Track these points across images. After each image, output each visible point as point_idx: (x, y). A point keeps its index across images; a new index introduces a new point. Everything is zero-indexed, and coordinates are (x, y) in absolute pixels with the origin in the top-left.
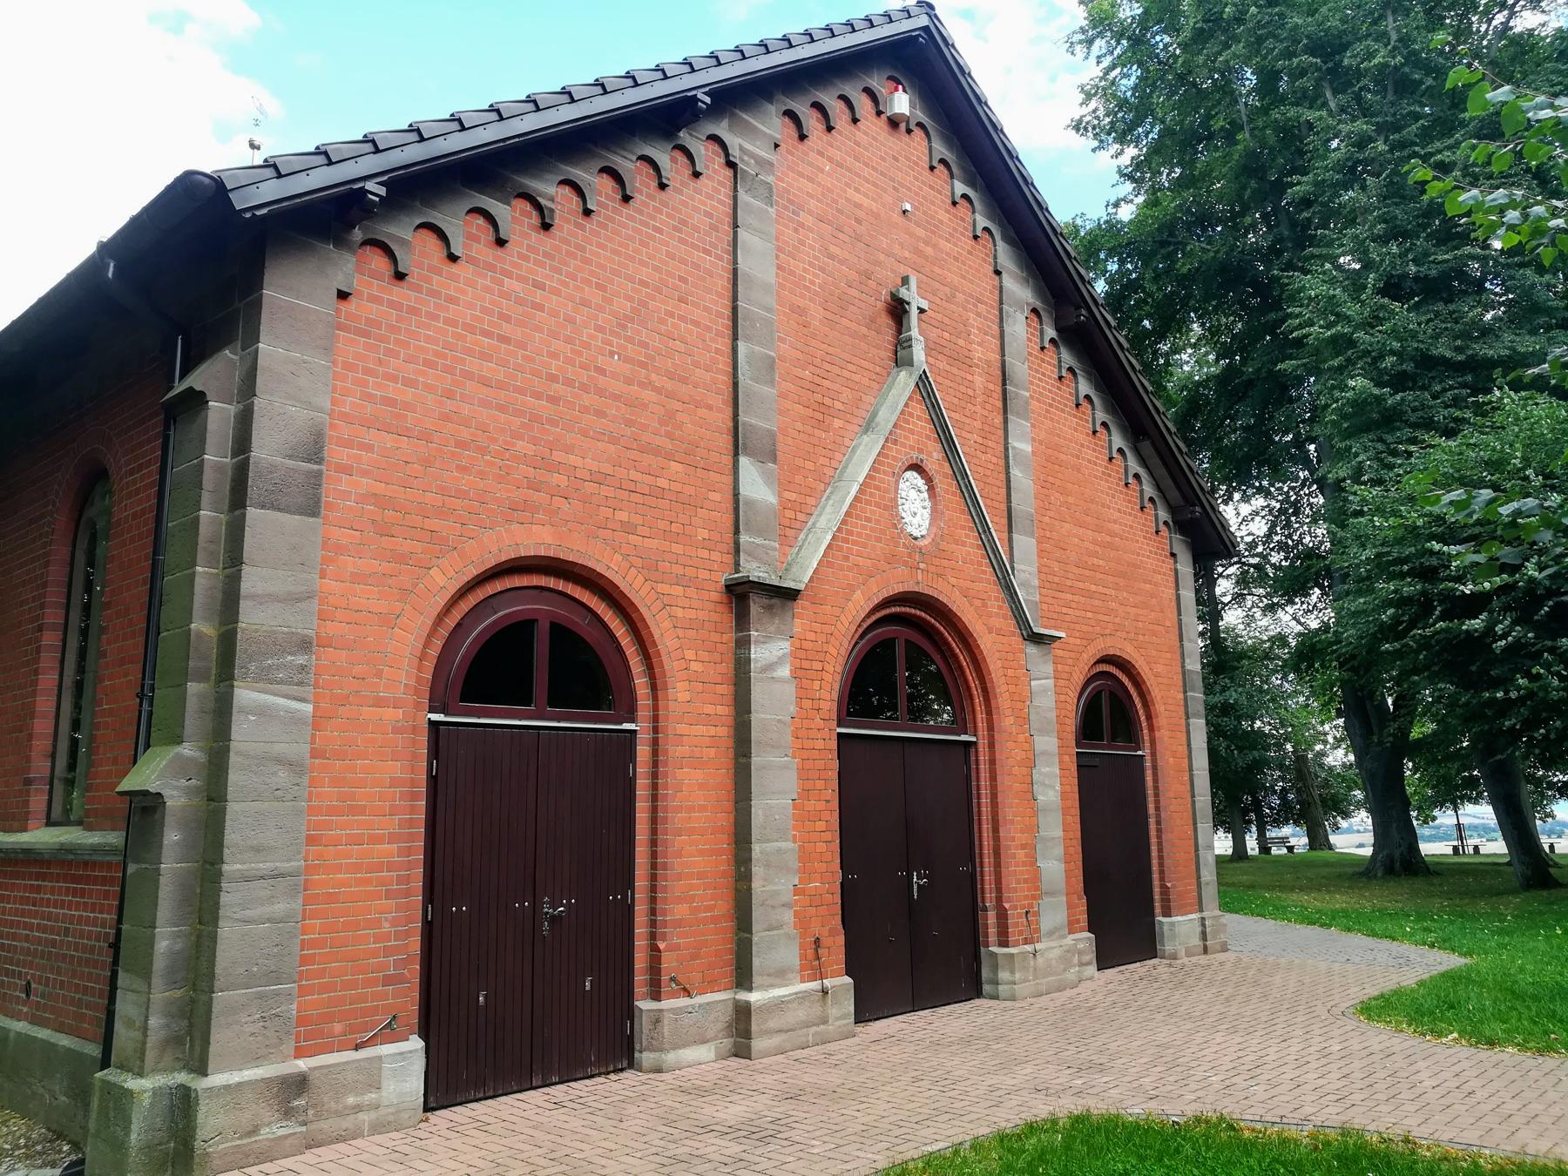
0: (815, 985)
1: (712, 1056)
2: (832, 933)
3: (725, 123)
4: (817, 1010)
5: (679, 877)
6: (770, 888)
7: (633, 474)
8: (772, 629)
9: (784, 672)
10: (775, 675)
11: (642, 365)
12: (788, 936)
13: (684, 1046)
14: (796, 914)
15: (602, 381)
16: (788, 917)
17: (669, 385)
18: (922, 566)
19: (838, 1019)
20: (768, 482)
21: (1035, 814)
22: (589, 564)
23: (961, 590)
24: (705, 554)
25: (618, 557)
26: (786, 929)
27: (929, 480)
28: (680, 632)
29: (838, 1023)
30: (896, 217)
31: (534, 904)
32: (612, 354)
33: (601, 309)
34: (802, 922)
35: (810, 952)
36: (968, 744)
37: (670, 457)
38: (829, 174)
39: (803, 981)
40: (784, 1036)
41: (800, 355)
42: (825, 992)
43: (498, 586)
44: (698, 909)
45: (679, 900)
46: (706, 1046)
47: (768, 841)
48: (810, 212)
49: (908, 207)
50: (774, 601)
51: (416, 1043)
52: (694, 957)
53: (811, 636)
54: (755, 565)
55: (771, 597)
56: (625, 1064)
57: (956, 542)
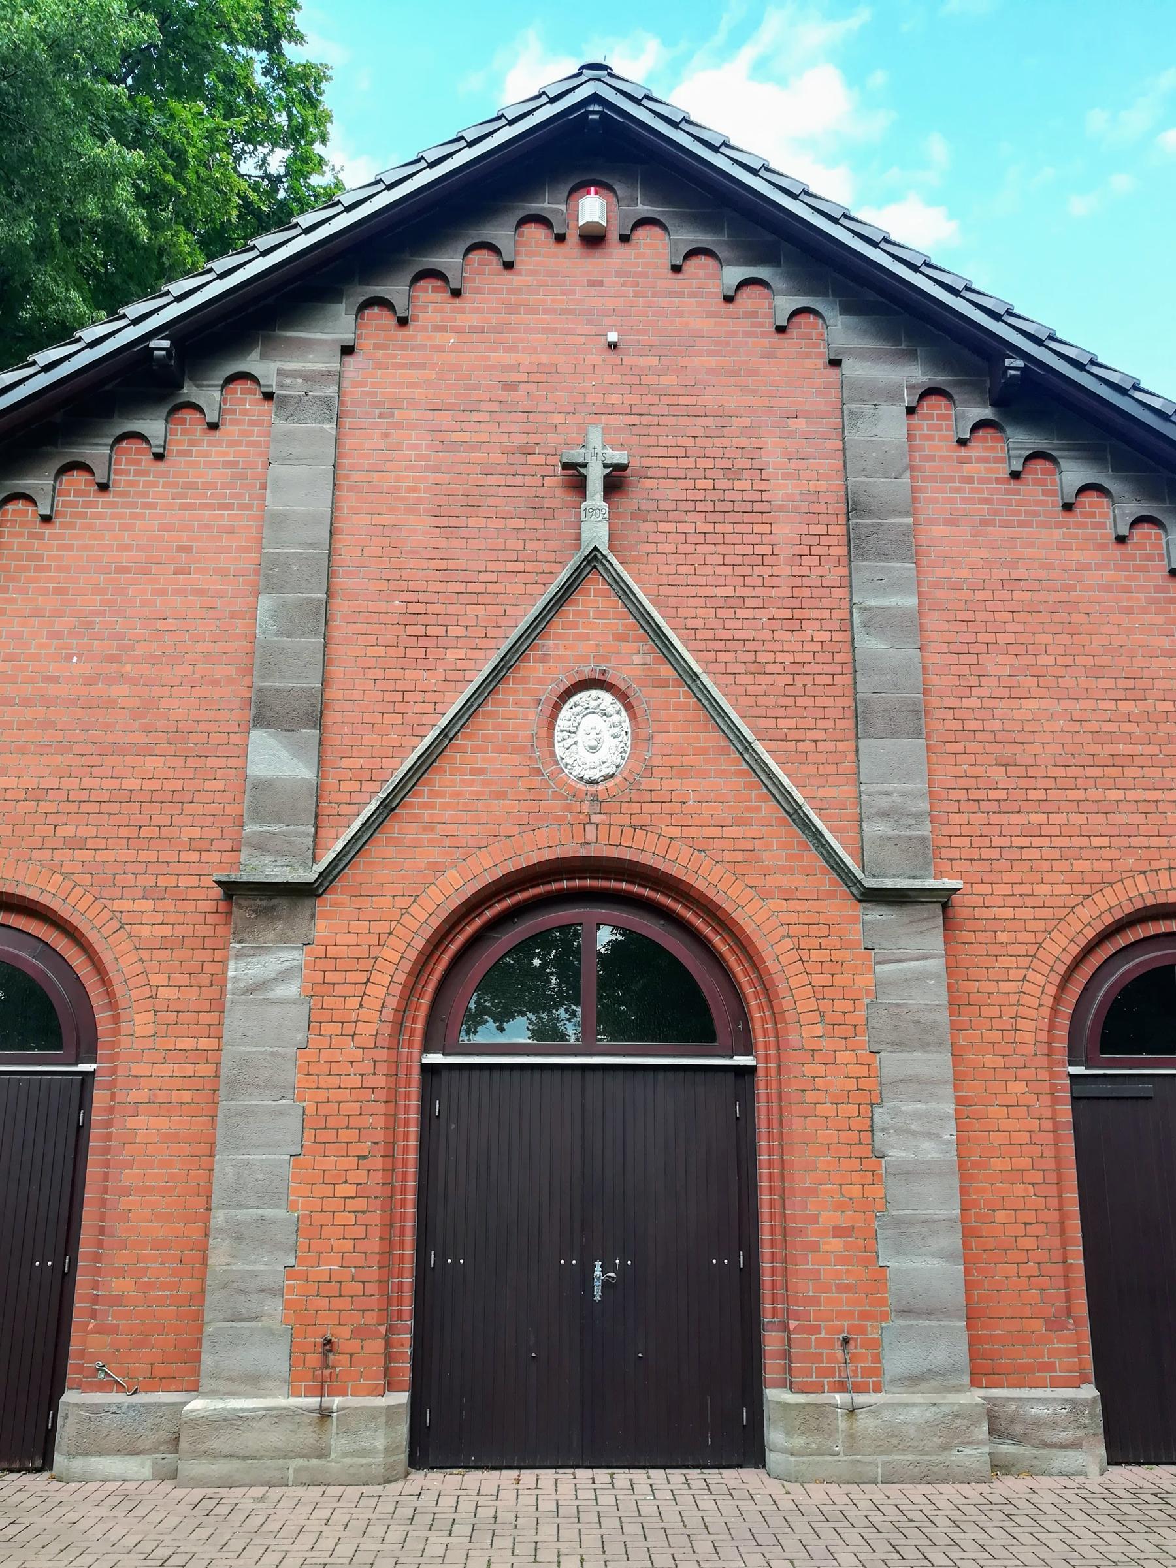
0: (313, 1402)
1: (147, 1472)
2: (359, 1334)
3: (255, 354)
4: (307, 1436)
5: (123, 1245)
6: (240, 1266)
7: (87, 782)
8: (271, 936)
9: (291, 989)
10: (271, 995)
11: (111, 659)
12: (270, 1332)
13: (100, 1453)
14: (288, 1304)
15: (51, 690)
16: (274, 1307)
17: (149, 671)
18: (595, 819)
19: (345, 1454)
20: (296, 755)
21: (877, 1179)
22: (17, 891)
23: (691, 842)
24: (194, 857)
25: (58, 878)
26: (265, 1322)
27: (622, 696)
28: (145, 955)
29: (348, 1460)
30: (598, 358)
31: (581, 1262)
32: (69, 658)
33: (59, 613)
34: (301, 1314)
35: (314, 1359)
36: (751, 1070)
37: (146, 751)
38: (454, 348)
39: (295, 1393)
40: (236, 1464)
41: (383, 585)
42: (324, 1414)
43: (1110, 948)
44: (150, 1285)
45: (120, 1273)
46: (139, 1458)
47: (240, 1206)
48: (413, 406)
49: (613, 337)
50: (275, 902)
51: (1089, 1392)
52: (139, 1344)
53: (343, 939)
54: (267, 859)
55: (271, 897)
56: (38, 1463)
57: (683, 774)
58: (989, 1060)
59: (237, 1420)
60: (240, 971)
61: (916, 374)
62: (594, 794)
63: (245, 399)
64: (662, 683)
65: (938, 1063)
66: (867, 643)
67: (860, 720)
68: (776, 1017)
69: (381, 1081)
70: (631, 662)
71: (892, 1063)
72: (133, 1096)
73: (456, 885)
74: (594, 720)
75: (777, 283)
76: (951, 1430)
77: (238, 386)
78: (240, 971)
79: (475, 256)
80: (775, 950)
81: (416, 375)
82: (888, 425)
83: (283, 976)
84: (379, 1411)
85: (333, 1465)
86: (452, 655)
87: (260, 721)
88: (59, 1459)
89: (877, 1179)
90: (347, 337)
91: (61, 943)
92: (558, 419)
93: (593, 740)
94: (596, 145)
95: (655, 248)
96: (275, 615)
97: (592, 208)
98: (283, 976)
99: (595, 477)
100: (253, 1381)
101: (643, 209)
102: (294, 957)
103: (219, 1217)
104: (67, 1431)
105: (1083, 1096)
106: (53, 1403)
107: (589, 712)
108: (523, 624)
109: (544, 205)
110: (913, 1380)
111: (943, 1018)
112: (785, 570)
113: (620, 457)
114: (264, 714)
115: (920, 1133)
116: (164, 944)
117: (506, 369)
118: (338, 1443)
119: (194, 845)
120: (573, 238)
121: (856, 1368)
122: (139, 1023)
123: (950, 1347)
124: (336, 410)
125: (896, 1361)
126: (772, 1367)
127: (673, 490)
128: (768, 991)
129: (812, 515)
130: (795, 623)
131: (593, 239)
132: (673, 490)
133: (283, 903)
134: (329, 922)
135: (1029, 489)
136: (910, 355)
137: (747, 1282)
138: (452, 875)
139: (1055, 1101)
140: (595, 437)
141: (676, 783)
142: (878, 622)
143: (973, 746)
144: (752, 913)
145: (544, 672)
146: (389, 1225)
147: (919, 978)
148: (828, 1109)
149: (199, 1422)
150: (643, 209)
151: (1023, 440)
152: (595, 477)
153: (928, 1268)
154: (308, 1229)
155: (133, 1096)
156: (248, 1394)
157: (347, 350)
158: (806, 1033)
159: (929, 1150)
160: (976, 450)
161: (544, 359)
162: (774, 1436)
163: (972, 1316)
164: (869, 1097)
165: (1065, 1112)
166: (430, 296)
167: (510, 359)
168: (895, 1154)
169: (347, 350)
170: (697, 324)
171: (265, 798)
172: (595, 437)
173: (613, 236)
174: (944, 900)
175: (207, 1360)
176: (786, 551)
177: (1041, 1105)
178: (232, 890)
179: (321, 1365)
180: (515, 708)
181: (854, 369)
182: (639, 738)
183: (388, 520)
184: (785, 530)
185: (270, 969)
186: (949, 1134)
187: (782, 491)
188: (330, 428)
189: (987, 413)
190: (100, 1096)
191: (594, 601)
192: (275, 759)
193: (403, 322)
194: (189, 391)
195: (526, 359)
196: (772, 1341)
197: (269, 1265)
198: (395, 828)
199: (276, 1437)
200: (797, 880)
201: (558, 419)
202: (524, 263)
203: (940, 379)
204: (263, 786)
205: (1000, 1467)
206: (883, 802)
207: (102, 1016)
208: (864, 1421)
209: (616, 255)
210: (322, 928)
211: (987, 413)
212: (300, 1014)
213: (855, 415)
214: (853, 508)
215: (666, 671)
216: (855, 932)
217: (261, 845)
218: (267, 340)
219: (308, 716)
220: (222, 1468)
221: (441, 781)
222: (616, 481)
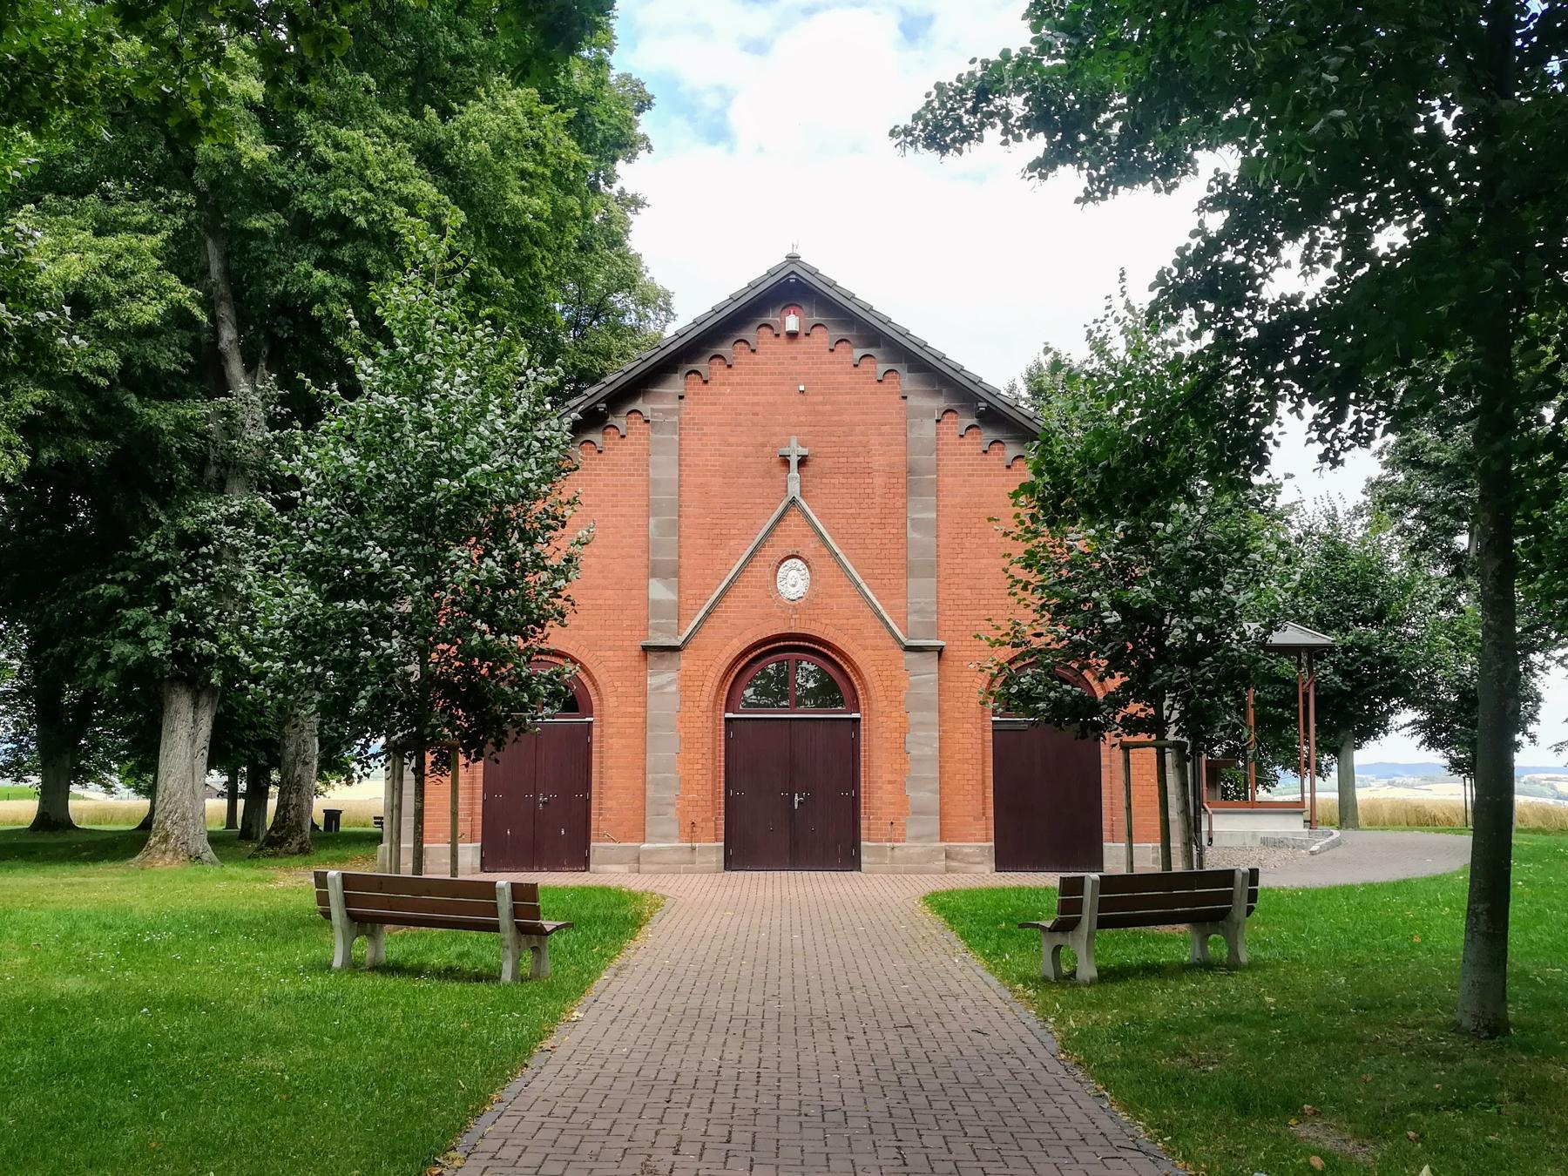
3: (640, 401)
4: (687, 857)
9: (673, 688)
16: (672, 811)
27: (806, 562)
35: (688, 829)
42: (693, 849)
57: (831, 596)
58: (957, 715)
59: (660, 851)
60: (652, 681)
61: (941, 403)
62: (794, 606)
63: (638, 422)
64: (822, 556)
65: (934, 716)
66: (913, 535)
67: (908, 570)
68: (869, 698)
69: (710, 724)
70: (810, 547)
71: (914, 717)
72: (611, 731)
73: (737, 645)
74: (793, 573)
75: (879, 357)
76: (931, 856)
77: (633, 415)
78: (652, 681)
79: (738, 345)
80: (868, 672)
81: (713, 409)
82: (928, 429)
83: (669, 683)
84: (713, 849)
85: (697, 866)
86: (732, 543)
87: (654, 575)
88: (592, 866)
89: (906, 762)
90: (681, 391)
91: (588, 684)
92: (777, 429)
93: (793, 581)
94: (792, 289)
95: (822, 338)
96: (657, 526)
97: (792, 323)
98: (669, 683)
99: (794, 461)
100: (665, 837)
101: (816, 319)
102: (673, 675)
103: (649, 777)
104: (595, 855)
105: (998, 730)
106: (587, 847)
107: (792, 569)
108: (765, 529)
109: (770, 318)
110: (918, 838)
111: (936, 698)
112: (878, 500)
113: (805, 452)
114: (654, 571)
115: (924, 743)
116: (619, 669)
117: (754, 404)
118: (698, 859)
119: (629, 628)
120: (783, 335)
121: (895, 831)
122: (611, 702)
123: (934, 825)
124: (680, 428)
125: (910, 832)
126: (1106, 835)
127: (829, 463)
128: (865, 688)
129: (891, 475)
130: (882, 526)
131: (793, 335)
132: (829, 463)
133: (668, 654)
134: (684, 661)
135: (992, 459)
136: (939, 393)
137: (856, 801)
138: (735, 641)
139: (984, 731)
140: (794, 441)
141: (829, 600)
142: (917, 524)
143: (957, 580)
144: (858, 656)
145: (773, 552)
146: (714, 778)
147: (927, 682)
148: (888, 735)
149: (646, 851)
150: (816, 319)
151: (988, 435)
152: (794, 461)
153: (925, 796)
154: (684, 781)
155: (611, 731)
156: (664, 841)
157: (681, 397)
158: (880, 704)
159: (928, 751)
160: (968, 439)
161: (771, 399)
162: (864, 858)
163: (943, 816)
164: (903, 730)
165: (989, 736)
166: (717, 366)
167: (755, 399)
168: (913, 752)
169: (681, 397)
170: (841, 378)
171: (657, 608)
172: (794, 441)
173: (802, 334)
174: (940, 651)
175: (648, 830)
176: (879, 491)
177: (977, 733)
178: (646, 649)
179: (691, 831)
180: (760, 568)
181: (914, 401)
182: (813, 582)
183: (703, 480)
184: (879, 481)
185: (663, 679)
186: (937, 745)
187: (878, 462)
188: (676, 437)
189: (974, 421)
190: (595, 731)
191: (793, 519)
192: (659, 591)
193: (706, 382)
194: (612, 420)
195: (762, 399)
196: (864, 824)
197: (670, 795)
198: (712, 621)
199: (675, 857)
200: (879, 642)
201: (777, 429)
202: (760, 348)
203: (953, 405)
204: (657, 602)
205: (948, 870)
206: (918, 606)
207: (594, 698)
208: (897, 852)
209: (804, 343)
210: (683, 663)
211: (974, 421)
212: (677, 699)
213: (912, 425)
214: (910, 471)
215: (825, 551)
216: (903, 664)
217: (657, 628)
218: (645, 394)
219: (672, 572)
220: (653, 868)
221: (729, 601)
222: (803, 461)
